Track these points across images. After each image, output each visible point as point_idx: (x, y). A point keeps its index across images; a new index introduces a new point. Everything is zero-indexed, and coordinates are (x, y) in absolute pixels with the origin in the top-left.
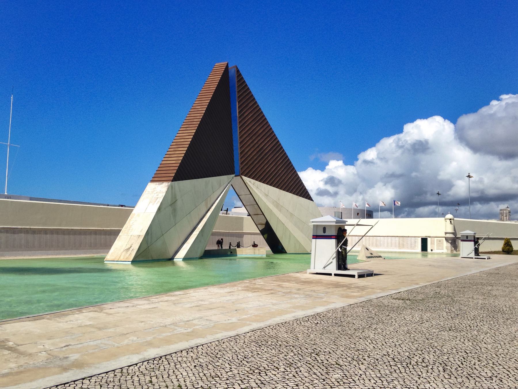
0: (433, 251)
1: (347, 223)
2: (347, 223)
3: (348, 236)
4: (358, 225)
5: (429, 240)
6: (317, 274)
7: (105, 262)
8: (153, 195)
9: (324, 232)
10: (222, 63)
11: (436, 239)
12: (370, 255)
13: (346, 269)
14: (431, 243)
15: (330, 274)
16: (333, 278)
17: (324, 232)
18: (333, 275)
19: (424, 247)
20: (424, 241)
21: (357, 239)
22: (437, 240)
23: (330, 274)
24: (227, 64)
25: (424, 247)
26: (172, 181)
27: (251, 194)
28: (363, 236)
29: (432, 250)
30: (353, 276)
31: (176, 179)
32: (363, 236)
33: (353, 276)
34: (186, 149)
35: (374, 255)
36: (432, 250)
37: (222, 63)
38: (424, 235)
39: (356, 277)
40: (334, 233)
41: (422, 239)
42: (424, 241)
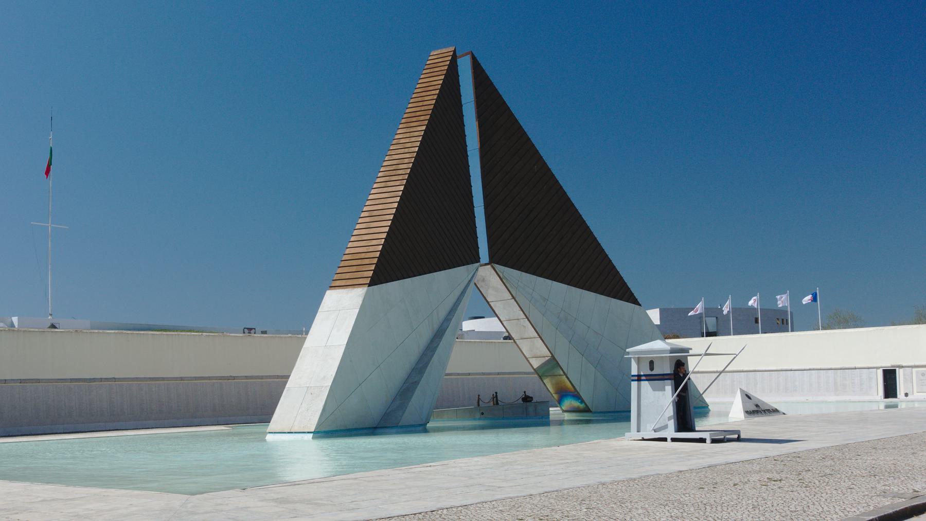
0: (910, 397)
1: (691, 352)
2: (311, 435)
3: (693, 372)
4: (706, 354)
5: (900, 376)
6: (643, 439)
7: (269, 437)
8: (338, 314)
9: (652, 369)
10: (444, 50)
11: (914, 370)
12: (755, 409)
13: (692, 429)
14: (905, 380)
15: (665, 440)
16: (669, 444)
17: (652, 369)
18: (669, 439)
19: (890, 389)
20: (890, 377)
21: (716, 375)
22: (917, 372)
23: (665, 440)
24: (455, 51)
25: (890, 389)
26: (370, 285)
28: (721, 373)
29: (906, 395)
30: (702, 440)
31: (377, 279)
32: (721, 373)
33: (702, 440)
34: (389, 223)
35: (763, 407)
36: (906, 395)
37: (444, 50)
38: (888, 364)
39: (708, 441)
40: (668, 369)
41: (884, 371)
42: (890, 377)
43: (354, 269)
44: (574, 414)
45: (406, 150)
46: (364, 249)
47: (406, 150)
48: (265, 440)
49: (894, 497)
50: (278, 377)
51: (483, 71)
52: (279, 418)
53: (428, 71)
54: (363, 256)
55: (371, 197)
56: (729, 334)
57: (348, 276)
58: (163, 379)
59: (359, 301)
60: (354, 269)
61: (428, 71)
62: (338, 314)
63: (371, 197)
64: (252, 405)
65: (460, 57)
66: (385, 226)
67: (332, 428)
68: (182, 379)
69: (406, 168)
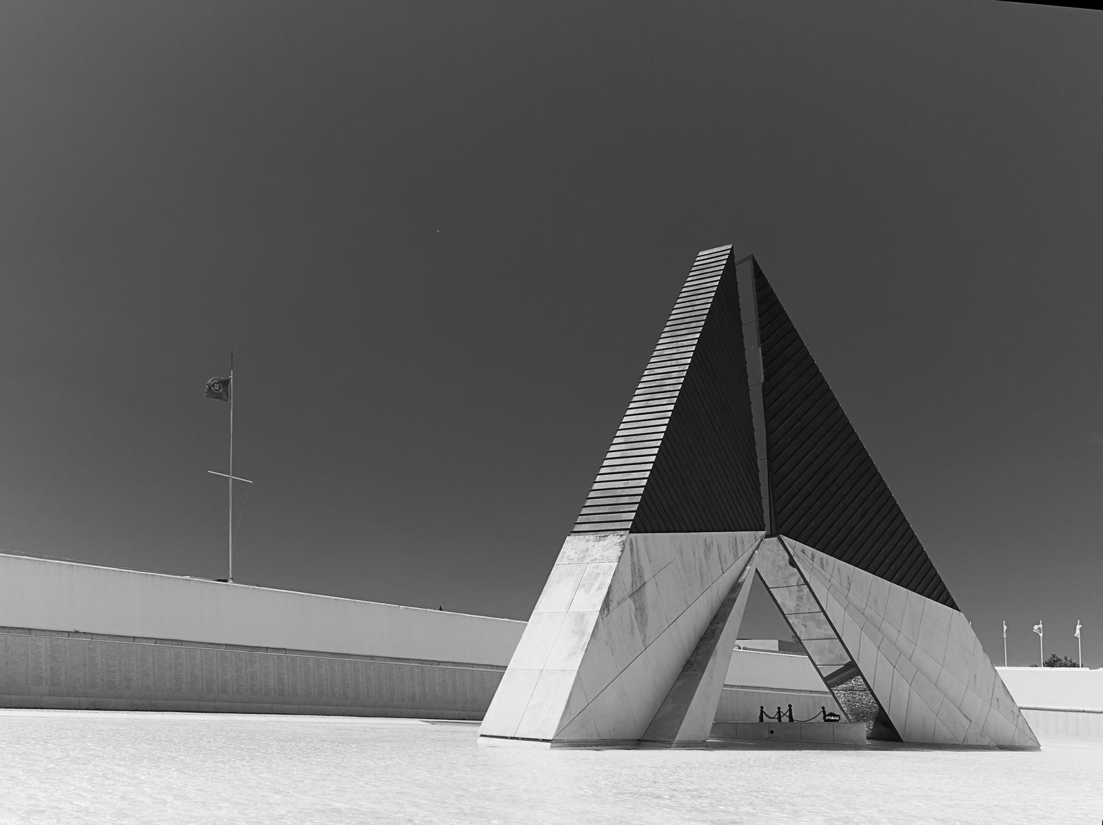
24: (732, 249)
27: (806, 583)
31: (638, 526)
43: (607, 509)
44: (872, 741)
45: (674, 363)
46: (621, 484)
47: (674, 363)
48: (476, 744)
49: (818, 813)
50: (498, 667)
51: (766, 283)
52: (494, 718)
53: (669, 334)
54: (619, 492)
55: (589, 503)
56: (1005, 666)
57: (597, 518)
58: (349, 655)
59: (616, 552)
60: (607, 509)
61: (669, 334)
62: (585, 569)
63: (589, 503)
64: (459, 698)
65: (740, 262)
66: (651, 455)
67: (585, 733)
68: (372, 657)
69: (675, 385)
